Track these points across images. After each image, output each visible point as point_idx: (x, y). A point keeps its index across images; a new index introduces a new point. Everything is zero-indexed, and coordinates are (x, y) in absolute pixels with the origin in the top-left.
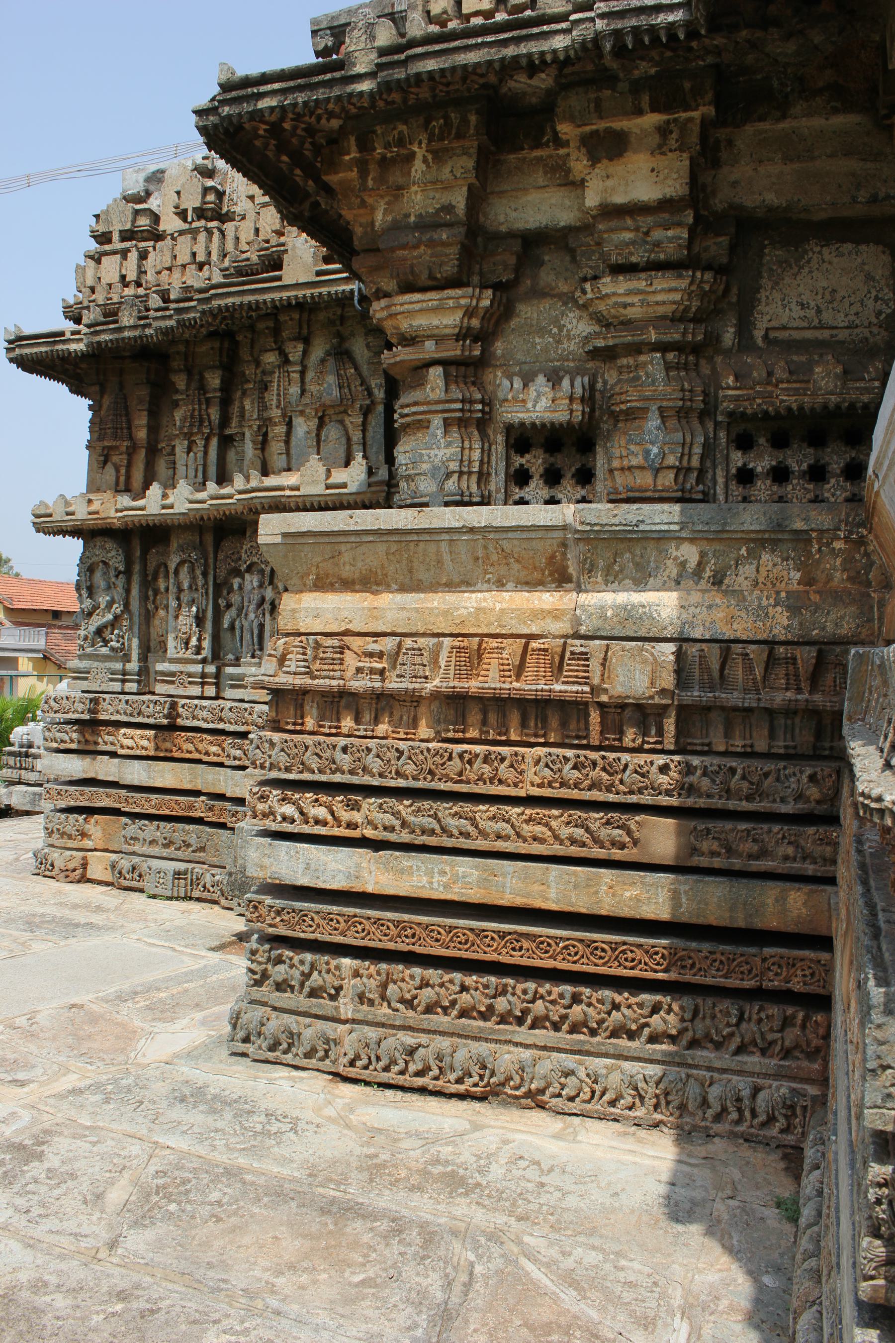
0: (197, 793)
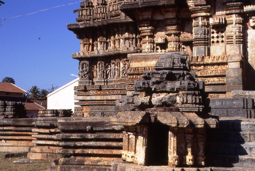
0: (104, 100)
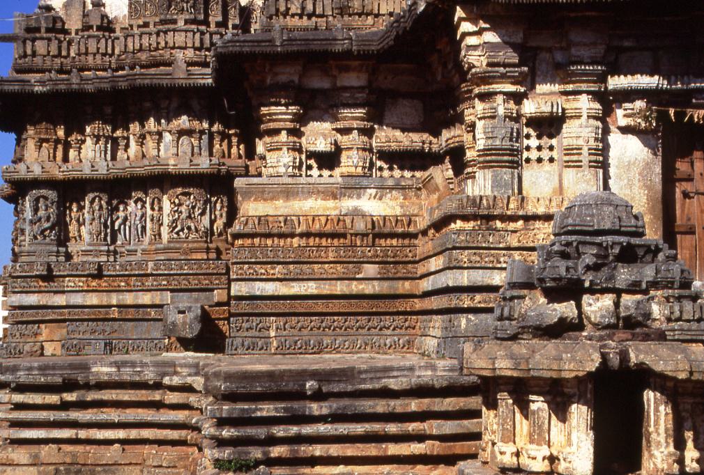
0: (110, 306)
